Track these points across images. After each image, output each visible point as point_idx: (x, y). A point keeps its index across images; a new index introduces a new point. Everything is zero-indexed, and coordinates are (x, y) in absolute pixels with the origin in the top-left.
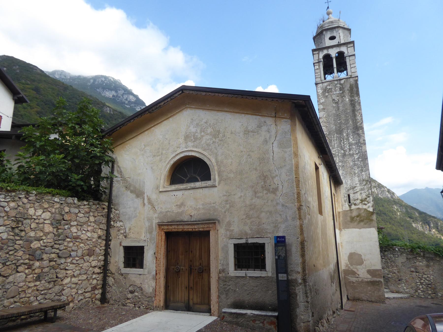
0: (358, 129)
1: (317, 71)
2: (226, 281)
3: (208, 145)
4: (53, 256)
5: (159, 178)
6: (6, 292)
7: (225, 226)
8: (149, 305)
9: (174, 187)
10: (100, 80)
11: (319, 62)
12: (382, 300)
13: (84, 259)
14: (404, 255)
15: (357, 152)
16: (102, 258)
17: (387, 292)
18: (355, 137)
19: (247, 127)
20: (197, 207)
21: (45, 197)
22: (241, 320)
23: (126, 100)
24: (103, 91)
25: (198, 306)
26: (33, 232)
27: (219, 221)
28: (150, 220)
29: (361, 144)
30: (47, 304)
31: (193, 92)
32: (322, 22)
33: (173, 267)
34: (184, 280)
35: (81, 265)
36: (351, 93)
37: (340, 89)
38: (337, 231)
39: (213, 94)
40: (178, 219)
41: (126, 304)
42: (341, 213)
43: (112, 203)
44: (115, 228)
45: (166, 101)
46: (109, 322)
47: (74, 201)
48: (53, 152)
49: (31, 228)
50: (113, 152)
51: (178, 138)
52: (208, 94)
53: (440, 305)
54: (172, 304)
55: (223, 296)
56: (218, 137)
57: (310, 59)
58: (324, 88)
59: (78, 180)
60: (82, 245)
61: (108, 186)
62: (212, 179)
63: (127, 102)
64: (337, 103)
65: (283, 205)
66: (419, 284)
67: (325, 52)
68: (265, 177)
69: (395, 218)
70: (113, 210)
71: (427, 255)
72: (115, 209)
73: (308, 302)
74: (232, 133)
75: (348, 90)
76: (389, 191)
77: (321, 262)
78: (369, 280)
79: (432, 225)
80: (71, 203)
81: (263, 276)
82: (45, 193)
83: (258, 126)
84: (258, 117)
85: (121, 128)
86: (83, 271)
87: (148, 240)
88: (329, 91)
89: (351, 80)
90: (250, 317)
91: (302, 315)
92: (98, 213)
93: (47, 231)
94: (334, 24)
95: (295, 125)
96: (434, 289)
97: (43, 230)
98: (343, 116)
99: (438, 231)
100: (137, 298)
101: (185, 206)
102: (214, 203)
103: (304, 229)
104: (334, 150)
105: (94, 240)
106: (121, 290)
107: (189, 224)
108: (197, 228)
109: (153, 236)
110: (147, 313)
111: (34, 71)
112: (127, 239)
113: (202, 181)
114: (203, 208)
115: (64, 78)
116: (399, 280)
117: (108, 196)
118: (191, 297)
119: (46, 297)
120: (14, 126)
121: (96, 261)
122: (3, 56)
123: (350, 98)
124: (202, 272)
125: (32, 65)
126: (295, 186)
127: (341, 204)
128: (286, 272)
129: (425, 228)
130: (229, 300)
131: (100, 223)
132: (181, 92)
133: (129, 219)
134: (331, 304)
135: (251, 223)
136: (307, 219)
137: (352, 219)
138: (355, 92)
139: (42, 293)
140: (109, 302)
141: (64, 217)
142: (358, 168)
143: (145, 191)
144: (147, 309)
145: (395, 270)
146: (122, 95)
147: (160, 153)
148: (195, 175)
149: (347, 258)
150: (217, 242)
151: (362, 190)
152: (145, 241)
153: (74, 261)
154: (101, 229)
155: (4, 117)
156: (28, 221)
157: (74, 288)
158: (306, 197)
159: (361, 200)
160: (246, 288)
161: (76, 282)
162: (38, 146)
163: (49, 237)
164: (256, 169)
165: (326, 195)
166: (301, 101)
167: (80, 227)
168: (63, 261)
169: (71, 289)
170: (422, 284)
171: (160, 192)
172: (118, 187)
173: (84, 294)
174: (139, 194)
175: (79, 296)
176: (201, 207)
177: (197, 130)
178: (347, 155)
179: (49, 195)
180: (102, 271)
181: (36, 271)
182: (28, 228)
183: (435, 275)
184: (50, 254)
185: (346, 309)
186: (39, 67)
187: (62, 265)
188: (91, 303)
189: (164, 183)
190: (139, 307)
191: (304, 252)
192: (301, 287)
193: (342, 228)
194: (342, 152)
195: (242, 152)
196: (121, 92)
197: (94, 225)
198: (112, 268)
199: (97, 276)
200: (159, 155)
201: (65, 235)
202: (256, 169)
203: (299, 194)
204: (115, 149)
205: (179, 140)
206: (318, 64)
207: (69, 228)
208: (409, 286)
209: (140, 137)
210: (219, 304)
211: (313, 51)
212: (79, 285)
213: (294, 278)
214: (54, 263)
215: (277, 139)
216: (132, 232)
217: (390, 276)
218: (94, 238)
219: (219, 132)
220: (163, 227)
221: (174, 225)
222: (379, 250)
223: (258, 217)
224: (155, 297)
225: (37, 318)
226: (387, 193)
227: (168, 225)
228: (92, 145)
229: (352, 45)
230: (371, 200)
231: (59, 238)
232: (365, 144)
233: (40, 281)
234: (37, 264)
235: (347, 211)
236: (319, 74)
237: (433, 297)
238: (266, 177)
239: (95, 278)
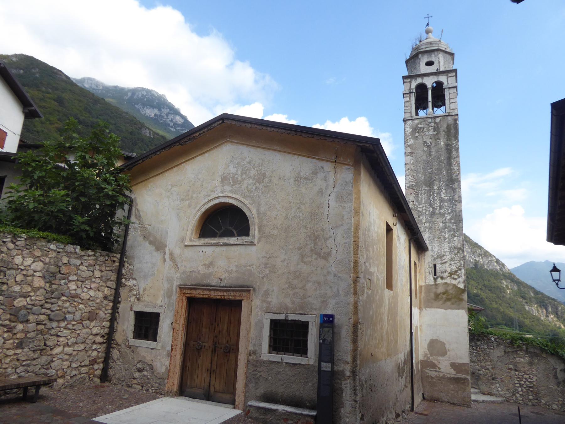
0: (453, 182)
1: (407, 104)
2: (256, 366)
3: (250, 191)
4: (42, 317)
9: (203, 241)
10: (140, 93)
11: (410, 93)
12: (466, 403)
13: (82, 324)
14: (502, 347)
15: (449, 211)
16: (107, 324)
17: (476, 393)
18: (449, 191)
19: (299, 173)
20: (230, 269)
21: (37, 242)
22: (269, 417)
23: (172, 121)
24: (143, 108)
26: (18, 286)
27: (254, 289)
28: (170, 280)
29: (456, 201)
30: (30, 378)
31: (236, 123)
32: (418, 43)
33: (193, 343)
34: (205, 360)
35: (78, 332)
36: (448, 136)
37: (434, 129)
38: (415, 311)
40: (205, 282)
41: (132, 384)
42: (423, 288)
43: (125, 255)
45: (202, 132)
46: (105, 406)
47: (75, 249)
48: (57, 185)
49: (16, 281)
50: (131, 191)
51: (214, 180)
53: (542, 415)
54: (188, 390)
55: (252, 385)
56: (263, 182)
57: (401, 88)
58: (414, 126)
59: (83, 223)
60: (81, 306)
61: (122, 234)
63: (172, 124)
64: (429, 147)
65: (335, 275)
66: (518, 385)
67: (419, 81)
69: (504, 297)
70: (126, 264)
71: (532, 350)
72: (128, 264)
73: (356, 401)
74: (280, 178)
75: (444, 131)
76: (498, 261)
77: (384, 349)
78: (453, 376)
79: (550, 310)
80: (71, 252)
81: (302, 363)
82: (38, 238)
84: (315, 161)
85: (143, 161)
86: (80, 339)
87: (166, 306)
88: (420, 131)
89: (449, 118)
90: (281, 414)
91: (347, 417)
92: (106, 266)
93: (37, 286)
95: (360, 174)
96: (537, 393)
97: (31, 284)
98: (435, 164)
99: (558, 318)
100: (145, 378)
101: (215, 266)
102: (250, 266)
103: (359, 308)
104: (420, 206)
105: (98, 301)
106: (126, 366)
107: (217, 290)
108: (227, 296)
109: (172, 301)
110: (154, 399)
111: (58, 76)
113: (239, 236)
114: (237, 271)
115: (95, 88)
116: (493, 379)
117: (122, 246)
118: (212, 383)
119: (29, 369)
120: (22, 146)
121: (97, 328)
122: (20, 55)
124: (229, 352)
125: (55, 69)
126: (352, 252)
127: (424, 276)
128: (331, 361)
129: (540, 312)
130: (258, 391)
131: (108, 279)
132: (221, 122)
133: (145, 277)
134: (395, 404)
135: (294, 295)
136: (366, 295)
137: (437, 297)
138: (453, 134)
139: (24, 363)
140: (110, 381)
141: (61, 269)
142: (449, 231)
143: (168, 244)
144: (157, 393)
145: (489, 365)
146: (167, 115)
147: (190, 197)
149: (426, 346)
150: (250, 315)
151: (452, 260)
152: (162, 306)
153: (70, 326)
154: (108, 287)
155: (9, 134)
156: (13, 272)
157: (67, 360)
158: (366, 266)
159: (450, 273)
160: (280, 377)
161: (70, 352)
162: (36, 177)
163: (38, 293)
164: (306, 227)
165: (402, 263)
166: (368, 145)
167: (81, 283)
168: (54, 324)
169: (63, 361)
170: (521, 386)
171: (186, 246)
172: (134, 236)
173: (80, 368)
174: (160, 246)
175: (72, 370)
176: (234, 269)
177: (237, 171)
178: (437, 214)
179: (42, 240)
180: (105, 341)
181: (18, 336)
182: (12, 280)
183: (539, 376)
184: (38, 315)
185: (418, 411)
186: (65, 73)
187: (53, 331)
188: (87, 380)
189: (192, 234)
190: (147, 391)
191: (357, 337)
192: (348, 381)
193: (423, 306)
194: (431, 209)
195: (290, 203)
196: (165, 111)
197: (99, 281)
198: (118, 337)
199: (99, 346)
201: (60, 292)
202: (306, 227)
203: (356, 262)
204: (133, 187)
205: (214, 182)
206: (408, 95)
207: (66, 284)
208: (505, 388)
210: (245, 395)
211: (404, 78)
212: (74, 356)
213: (341, 369)
214: (43, 327)
215: (335, 190)
216: (146, 294)
217: (481, 373)
218: (99, 298)
219: (264, 175)
221: (199, 289)
222: (467, 338)
223: (303, 288)
224: (168, 379)
225: (14, 395)
226: (495, 264)
227: (191, 289)
228: (105, 180)
229: (454, 74)
230: (463, 274)
231: (52, 295)
232: (460, 201)
233: (23, 348)
234: (20, 327)
235: (431, 285)
236: (409, 108)
237: (535, 404)
238: (316, 238)
239: (95, 349)
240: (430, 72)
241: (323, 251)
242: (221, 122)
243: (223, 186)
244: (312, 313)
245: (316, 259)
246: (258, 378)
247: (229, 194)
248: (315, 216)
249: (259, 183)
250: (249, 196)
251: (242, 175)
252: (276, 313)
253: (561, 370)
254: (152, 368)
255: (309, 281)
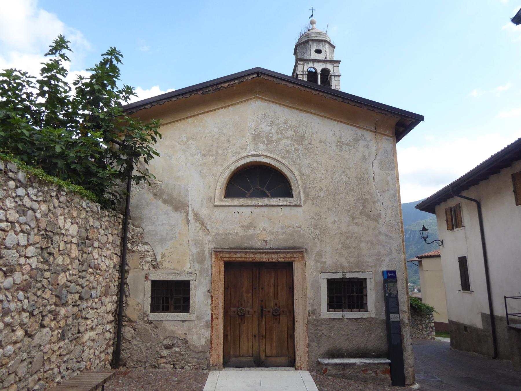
2: (317, 325)
5: (212, 186)
6: (31, 363)
7: (315, 257)
8: (199, 364)
11: (303, 74)
19: (340, 138)
20: (275, 231)
22: (349, 372)
25: (273, 359)
27: (306, 250)
33: (233, 309)
34: (251, 327)
39: (303, 89)
40: (246, 245)
44: (135, 254)
52: (295, 86)
54: (233, 360)
55: (314, 345)
56: (302, 144)
62: (294, 196)
65: (386, 235)
68: (365, 201)
72: (134, 226)
74: (321, 142)
81: (364, 317)
83: (354, 139)
84: (355, 128)
90: (359, 367)
100: (177, 355)
101: (255, 227)
106: (148, 345)
114: (283, 233)
118: (262, 348)
124: (279, 315)
132: (256, 76)
133: (162, 241)
135: (348, 254)
143: (190, 203)
147: (214, 153)
150: (304, 277)
152: (191, 273)
160: (343, 333)
164: (353, 190)
174: (179, 205)
177: (271, 130)
190: (183, 368)
192: (407, 328)
198: (131, 312)
200: (212, 155)
202: (353, 190)
205: (244, 139)
209: (179, 124)
215: (377, 157)
219: (303, 137)
220: (221, 255)
221: (240, 252)
223: (357, 247)
242: (256, 76)
243: (256, 144)
244: (368, 270)
245: (367, 221)
246: (320, 336)
249: (298, 145)
250: (288, 157)
252: (332, 273)
254: (187, 342)
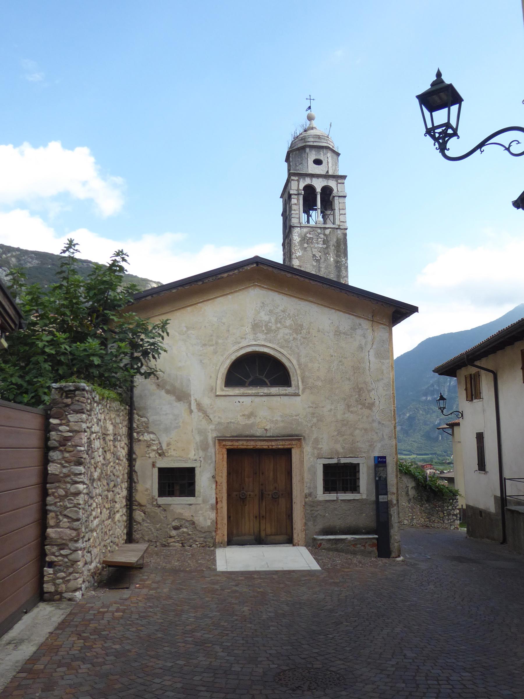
7: (312, 443)
8: (205, 542)
9: (231, 391)
11: (298, 194)
19: (338, 327)
20: (274, 419)
22: (340, 546)
25: (273, 537)
27: (304, 437)
33: (235, 493)
36: (337, 251)
37: (324, 241)
40: (247, 433)
44: (142, 443)
51: (243, 326)
54: (235, 539)
55: (310, 523)
56: (301, 333)
58: (303, 235)
62: (293, 386)
64: (318, 261)
65: (379, 423)
67: (308, 181)
68: (360, 389)
72: (139, 416)
74: (319, 331)
81: (356, 498)
84: (352, 317)
87: (201, 459)
88: (309, 241)
89: (339, 232)
90: (350, 541)
94: (322, 141)
100: (185, 535)
101: (256, 416)
102: (296, 416)
108: (274, 445)
112: (165, 458)
114: (282, 421)
118: (263, 528)
123: (336, 258)
133: (167, 430)
138: (342, 250)
143: (192, 393)
147: (214, 342)
148: (261, 377)
150: (302, 462)
160: (336, 512)
174: (181, 395)
177: (270, 319)
195: (332, 356)
198: (140, 497)
200: (212, 345)
205: (244, 328)
206: (296, 197)
215: (374, 346)
216: (172, 449)
219: (301, 326)
220: (224, 443)
221: (242, 440)
223: (352, 434)
236: (297, 212)
240: (318, 173)
241: (367, 402)
246: (316, 516)
247: (263, 343)
248: (357, 369)
250: (287, 347)
251: (276, 324)
253: (412, 488)
254: (193, 523)
255: (356, 428)
